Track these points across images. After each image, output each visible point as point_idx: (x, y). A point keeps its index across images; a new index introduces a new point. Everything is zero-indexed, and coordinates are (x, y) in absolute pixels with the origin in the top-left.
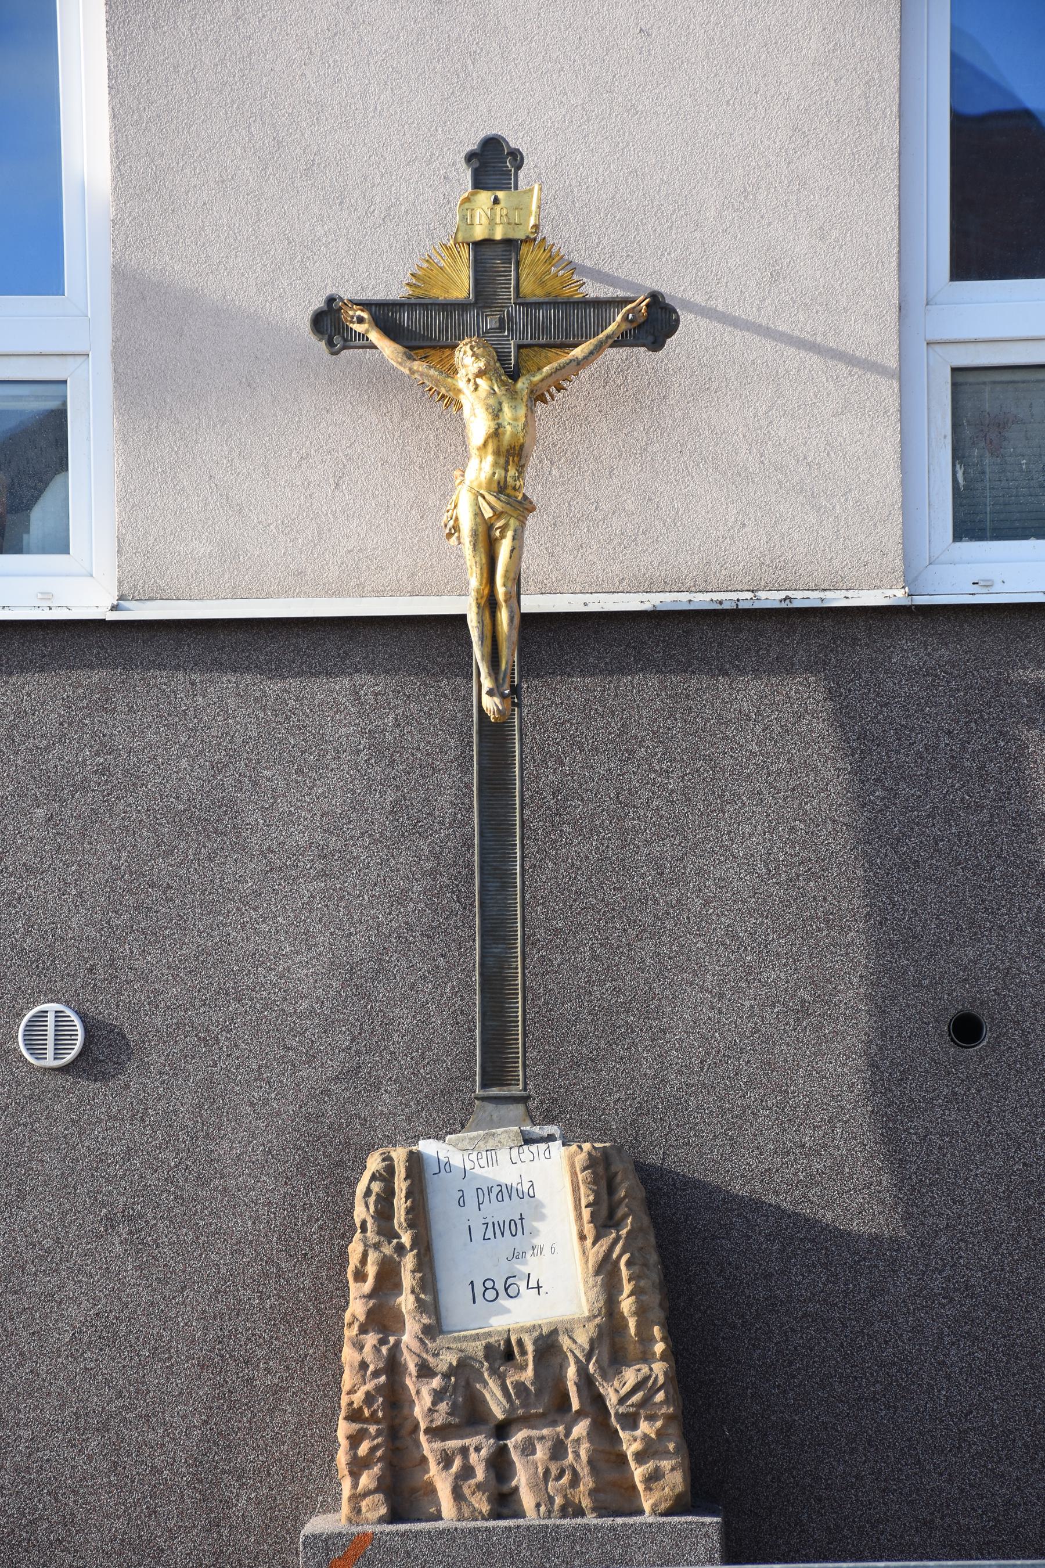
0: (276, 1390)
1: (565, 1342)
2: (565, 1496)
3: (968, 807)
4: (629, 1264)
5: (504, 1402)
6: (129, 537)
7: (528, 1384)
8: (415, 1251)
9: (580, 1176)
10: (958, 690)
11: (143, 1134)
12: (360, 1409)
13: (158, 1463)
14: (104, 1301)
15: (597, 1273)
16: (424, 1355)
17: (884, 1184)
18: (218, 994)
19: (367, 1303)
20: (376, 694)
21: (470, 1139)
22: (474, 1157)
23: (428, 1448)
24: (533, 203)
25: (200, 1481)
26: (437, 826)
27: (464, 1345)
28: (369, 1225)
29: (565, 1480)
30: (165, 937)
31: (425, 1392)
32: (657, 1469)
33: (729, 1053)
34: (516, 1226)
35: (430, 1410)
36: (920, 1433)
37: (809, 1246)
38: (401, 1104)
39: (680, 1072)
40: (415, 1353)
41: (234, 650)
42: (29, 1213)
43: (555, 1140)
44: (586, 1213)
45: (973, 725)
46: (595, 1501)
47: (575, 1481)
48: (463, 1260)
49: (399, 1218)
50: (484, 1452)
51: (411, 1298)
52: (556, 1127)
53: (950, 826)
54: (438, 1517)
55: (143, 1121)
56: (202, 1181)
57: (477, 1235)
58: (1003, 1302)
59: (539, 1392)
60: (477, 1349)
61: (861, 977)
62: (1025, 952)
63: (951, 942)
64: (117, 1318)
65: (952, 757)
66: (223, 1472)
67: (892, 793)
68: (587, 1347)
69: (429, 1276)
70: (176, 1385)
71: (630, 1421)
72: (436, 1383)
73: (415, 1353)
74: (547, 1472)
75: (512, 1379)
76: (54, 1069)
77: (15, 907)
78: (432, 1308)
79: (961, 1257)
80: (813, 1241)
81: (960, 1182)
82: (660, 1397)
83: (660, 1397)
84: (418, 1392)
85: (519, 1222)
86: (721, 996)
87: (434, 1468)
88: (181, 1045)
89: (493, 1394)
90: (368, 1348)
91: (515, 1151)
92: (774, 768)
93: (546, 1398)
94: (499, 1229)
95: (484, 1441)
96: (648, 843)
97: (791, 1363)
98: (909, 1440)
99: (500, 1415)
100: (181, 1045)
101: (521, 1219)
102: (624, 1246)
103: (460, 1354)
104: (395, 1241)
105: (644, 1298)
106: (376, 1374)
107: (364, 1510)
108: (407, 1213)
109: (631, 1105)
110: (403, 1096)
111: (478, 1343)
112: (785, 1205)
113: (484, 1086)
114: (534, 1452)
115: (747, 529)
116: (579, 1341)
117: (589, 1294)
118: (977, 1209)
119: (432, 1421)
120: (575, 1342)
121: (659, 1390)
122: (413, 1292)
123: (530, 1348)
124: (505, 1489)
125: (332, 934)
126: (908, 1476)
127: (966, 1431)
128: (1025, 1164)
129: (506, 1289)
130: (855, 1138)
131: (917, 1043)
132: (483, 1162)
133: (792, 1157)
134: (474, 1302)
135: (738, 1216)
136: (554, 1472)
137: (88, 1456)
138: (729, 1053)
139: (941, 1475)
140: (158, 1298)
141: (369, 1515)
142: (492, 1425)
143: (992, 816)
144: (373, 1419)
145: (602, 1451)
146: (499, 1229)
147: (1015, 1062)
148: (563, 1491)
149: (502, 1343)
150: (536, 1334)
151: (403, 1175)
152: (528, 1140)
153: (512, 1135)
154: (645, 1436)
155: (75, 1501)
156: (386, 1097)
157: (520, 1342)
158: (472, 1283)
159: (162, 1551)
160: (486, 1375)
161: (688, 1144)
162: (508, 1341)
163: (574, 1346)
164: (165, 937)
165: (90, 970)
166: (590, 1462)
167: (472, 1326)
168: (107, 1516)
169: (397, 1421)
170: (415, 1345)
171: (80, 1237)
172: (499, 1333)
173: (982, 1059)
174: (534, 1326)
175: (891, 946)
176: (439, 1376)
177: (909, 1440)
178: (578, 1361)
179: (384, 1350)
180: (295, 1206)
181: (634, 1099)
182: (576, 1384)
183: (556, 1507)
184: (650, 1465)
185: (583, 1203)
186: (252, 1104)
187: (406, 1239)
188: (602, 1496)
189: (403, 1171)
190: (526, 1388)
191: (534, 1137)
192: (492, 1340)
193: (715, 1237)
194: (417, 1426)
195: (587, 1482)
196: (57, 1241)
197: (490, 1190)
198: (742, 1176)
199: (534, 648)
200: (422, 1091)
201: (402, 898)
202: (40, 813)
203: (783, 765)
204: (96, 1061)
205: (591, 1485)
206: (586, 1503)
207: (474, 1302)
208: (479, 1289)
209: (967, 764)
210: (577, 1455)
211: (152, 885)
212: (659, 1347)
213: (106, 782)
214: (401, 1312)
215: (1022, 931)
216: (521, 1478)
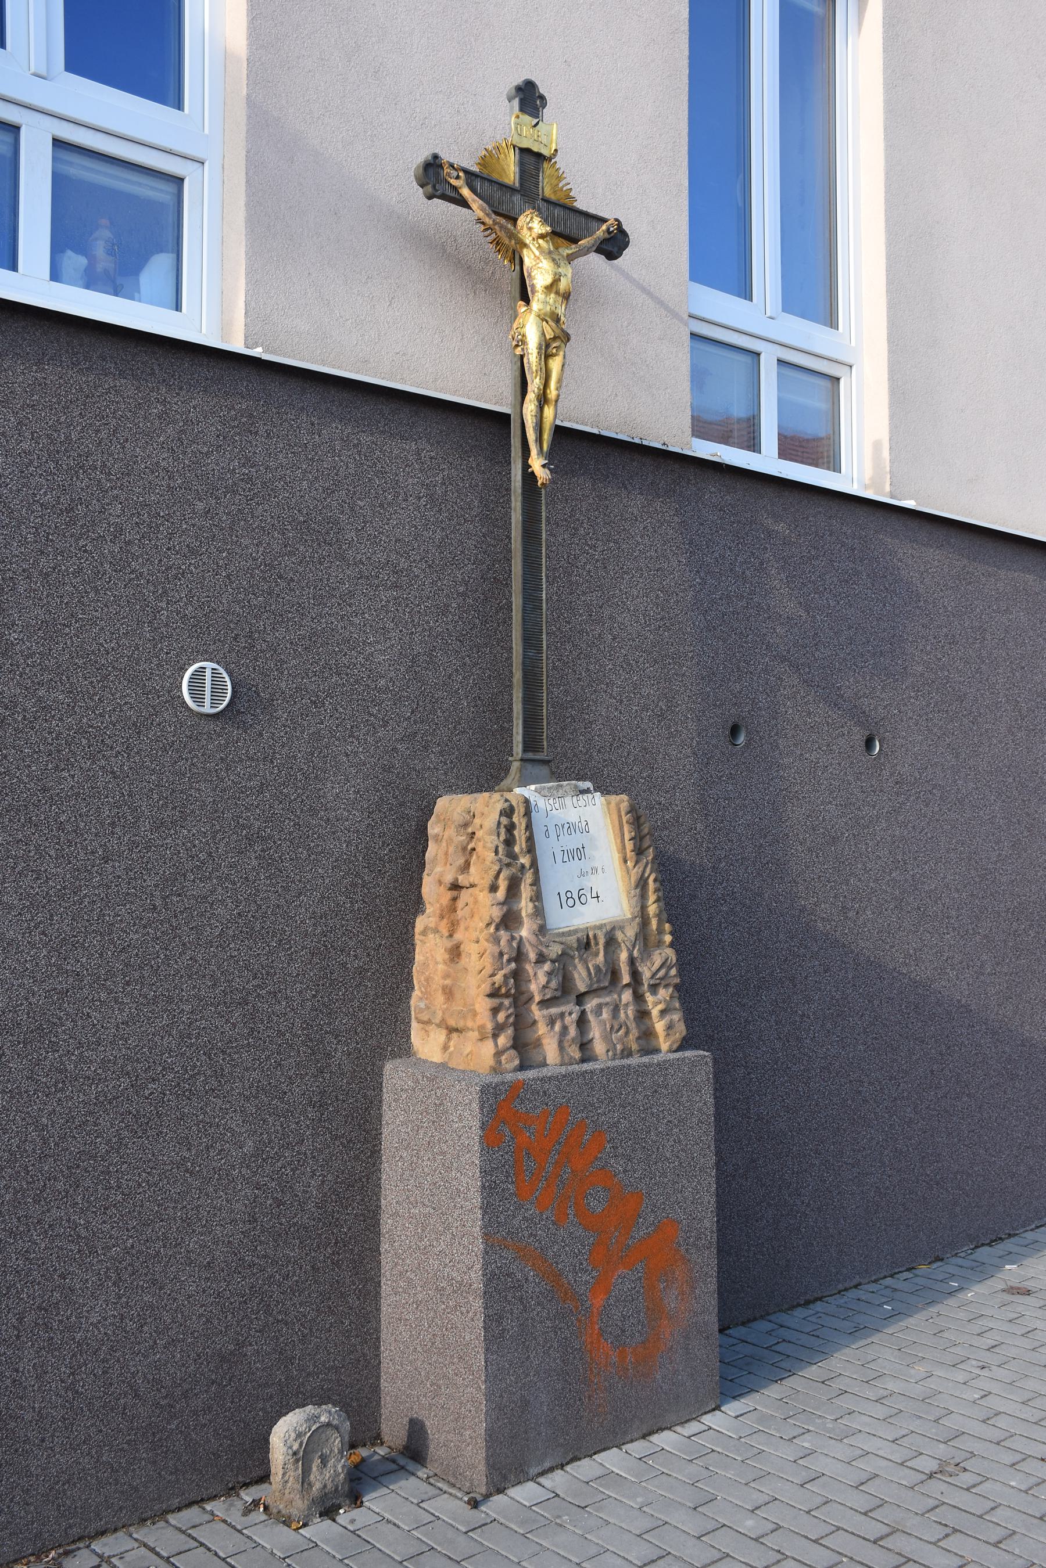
0: (361, 971)
1: (619, 935)
4: (655, 880)
6: (253, 304)
11: (272, 773)
12: (500, 988)
13: (283, 1029)
14: (244, 903)
15: (636, 887)
18: (325, 668)
19: (501, 909)
20: (431, 458)
23: (537, 1013)
24: (550, 134)
25: (311, 1040)
26: (466, 562)
27: (563, 939)
28: (500, 849)
30: (288, 620)
34: (579, 853)
39: (599, 751)
41: (341, 405)
42: (189, 831)
44: (629, 845)
48: (558, 877)
50: (573, 1016)
54: (544, 1064)
55: (272, 762)
56: (313, 812)
57: (559, 859)
60: (572, 940)
64: (253, 917)
66: (327, 1032)
67: (704, 582)
68: (633, 939)
70: (294, 968)
71: (654, 988)
74: (612, 1028)
76: (208, 715)
77: (180, 580)
84: (535, 974)
86: (621, 701)
87: (542, 1029)
88: (299, 705)
89: (580, 974)
90: (503, 943)
96: (584, 593)
100: (299, 705)
102: (652, 868)
107: (503, 1062)
113: (525, 751)
114: (601, 1015)
123: (602, 941)
124: (585, 1040)
125: (401, 631)
132: (557, 806)
136: (616, 1027)
137: (233, 1024)
138: (624, 740)
140: (282, 902)
141: (507, 1066)
144: (507, 995)
148: (620, 1040)
150: (604, 930)
155: (223, 1059)
156: (432, 756)
157: (595, 936)
159: (285, 1093)
164: (288, 620)
165: (235, 639)
167: (563, 925)
168: (247, 1069)
171: (227, 852)
172: (582, 930)
175: (703, 678)
178: (628, 949)
179: (515, 944)
180: (373, 834)
183: (618, 1052)
184: (667, 1018)
186: (347, 755)
192: (579, 935)
194: (531, 998)
196: (210, 854)
197: (563, 826)
201: (445, 611)
202: (200, 506)
204: (239, 712)
205: (637, 1035)
206: (635, 1047)
211: (281, 577)
212: (668, 938)
213: (250, 490)
216: (595, 1032)
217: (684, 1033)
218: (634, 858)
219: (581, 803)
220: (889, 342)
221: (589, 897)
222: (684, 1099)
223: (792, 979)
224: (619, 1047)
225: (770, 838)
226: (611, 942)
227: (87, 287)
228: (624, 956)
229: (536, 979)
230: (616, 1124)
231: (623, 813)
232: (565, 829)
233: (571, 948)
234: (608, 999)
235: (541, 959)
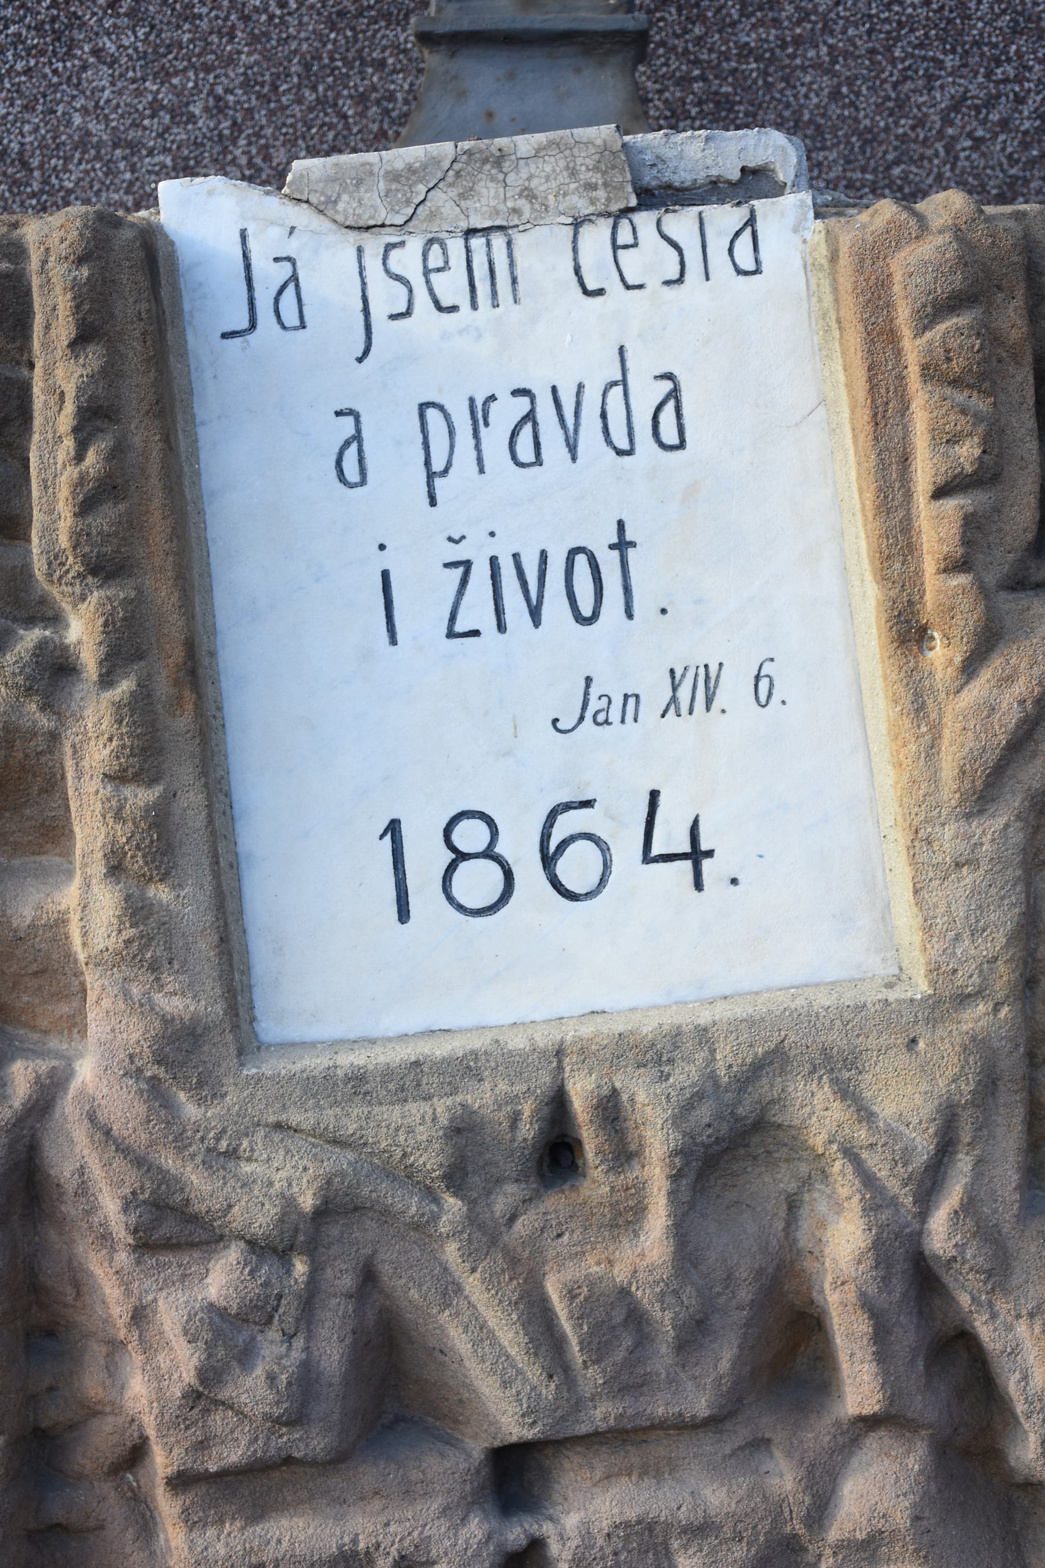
1: (817, 1113)
5: (534, 1373)
7: (644, 1295)
8: (125, 686)
9: (913, 350)
16: (169, 1161)
21: (394, 176)
22: (408, 260)
31: (171, 1314)
35: (193, 1397)
38: (156, 107)
40: (123, 1149)
43: (778, 190)
44: (937, 527)
49: (49, 530)
51: (107, 901)
52: (777, 138)
57: (422, 607)
59: (694, 1335)
69: (191, 800)
72: (221, 1279)
73: (123, 1149)
75: (572, 1272)
78: (205, 946)
84: (140, 1316)
85: (609, 562)
89: (482, 1334)
91: (596, 238)
94: (517, 588)
95: (437, 1529)
99: (513, 1426)
101: (622, 546)
103: (343, 1159)
104: (31, 637)
108: (86, 507)
109: (1004, 124)
110: (164, 76)
111: (416, 1109)
116: (887, 1110)
117: (936, 896)
119: (202, 1445)
120: (866, 1115)
122: (115, 869)
123: (658, 1142)
129: (548, 861)
132: (451, 286)
134: (404, 914)
142: (477, 1448)
146: (517, 588)
149: (527, 1109)
150: (685, 1075)
151: (64, 330)
152: (657, 195)
153: (584, 159)
156: (100, 77)
157: (611, 1110)
158: (394, 828)
160: (451, 1252)
162: (558, 1103)
163: (862, 1134)
169: (53, 1414)
170: (123, 1108)
172: (513, 1064)
174: (676, 1036)
176: (234, 1253)
181: (1020, 100)
182: (867, 1304)
185: (924, 474)
187: (81, 630)
189: (64, 302)
190: (636, 1318)
191: (683, 177)
192: (481, 1097)
197: (479, 414)
200: (230, 61)
207: (404, 914)
208: (425, 859)
214: (69, 956)
218: (967, 618)
219: (648, 259)
226: (734, 1143)
228: (842, 1243)
229: (147, 1348)
231: (903, 314)
232: (495, 438)
233: (408, 1176)
235: (171, 1229)
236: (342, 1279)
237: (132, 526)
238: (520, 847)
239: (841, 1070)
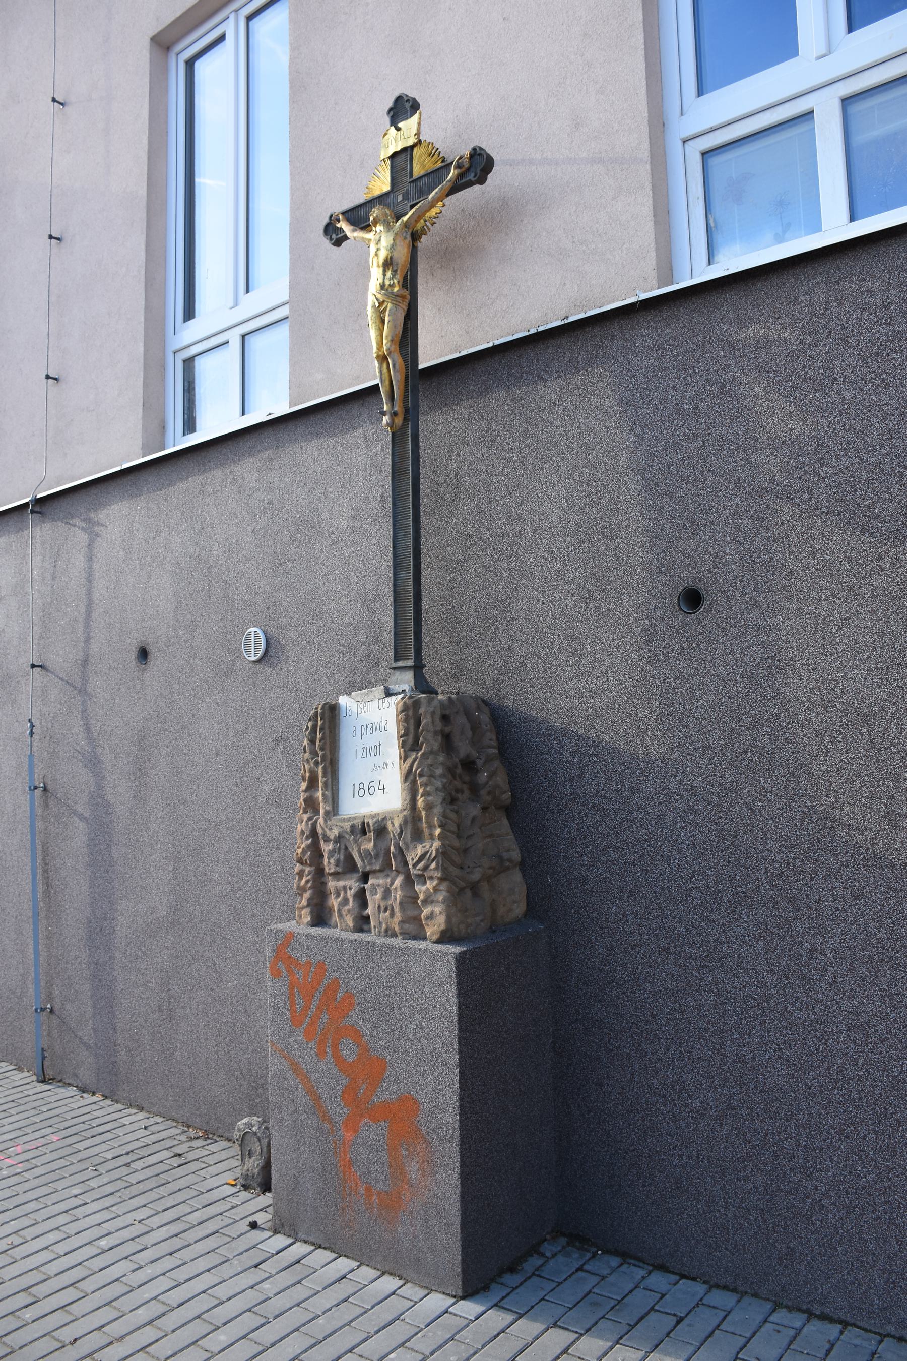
2: (387, 924)
3: (689, 438)
10: (678, 356)
17: (640, 715)
22: (362, 706)
29: (388, 914)
32: (432, 913)
33: (548, 630)
36: (662, 889)
37: (595, 759)
45: (689, 378)
46: (401, 928)
47: (392, 915)
53: (677, 454)
57: (359, 756)
58: (715, 799)
61: (624, 570)
62: (728, 539)
63: (680, 537)
65: (677, 404)
78: (330, 800)
79: (688, 766)
80: (597, 756)
81: (687, 712)
82: (433, 865)
83: (433, 865)
86: (543, 592)
92: (570, 434)
93: (381, 860)
97: (585, 837)
98: (655, 893)
105: (430, 798)
106: (307, 838)
112: (581, 732)
115: (568, 286)
118: (698, 731)
121: (433, 860)
126: (654, 918)
127: (691, 890)
128: (729, 697)
130: (621, 684)
131: (659, 613)
132: (366, 709)
133: (584, 698)
135: (555, 739)
138: (548, 630)
139: (674, 918)
143: (704, 442)
145: (410, 897)
147: (722, 622)
150: (375, 819)
154: (428, 889)
157: (368, 823)
161: (527, 692)
162: (364, 822)
166: (401, 903)
172: (359, 817)
173: (700, 621)
177: (655, 893)
188: (406, 926)
192: (355, 822)
193: (542, 753)
195: (398, 916)
198: (557, 712)
199: (444, 388)
203: (575, 431)
205: (400, 919)
208: (357, 789)
209: (686, 407)
210: (396, 899)
215: (726, 523)
217: (443, 927)
220: (290, 253)
221: (377, 788)
222: (426, 989)
223: (793, 902)
224: (384, 926)
225: (746, 720)
227: (780, 242)
230: (363, 992)
234: (381, 881)
236: (343, 847)
237: (325, 743)
238: (366, 788)
239: (391, 818)
